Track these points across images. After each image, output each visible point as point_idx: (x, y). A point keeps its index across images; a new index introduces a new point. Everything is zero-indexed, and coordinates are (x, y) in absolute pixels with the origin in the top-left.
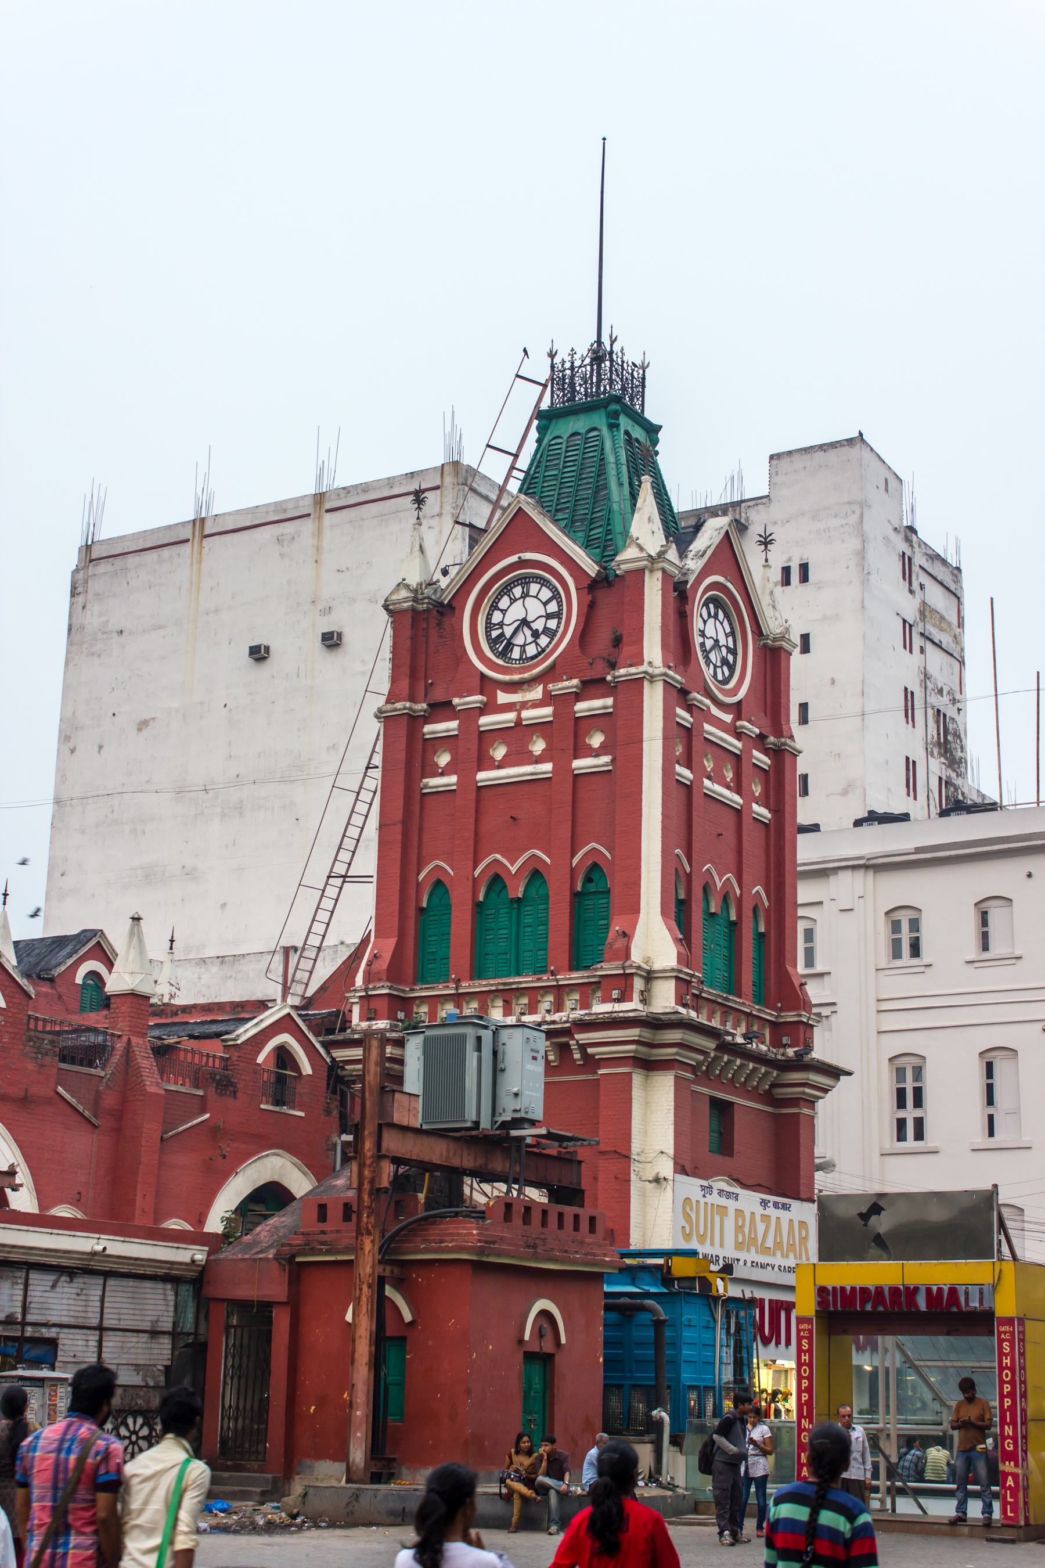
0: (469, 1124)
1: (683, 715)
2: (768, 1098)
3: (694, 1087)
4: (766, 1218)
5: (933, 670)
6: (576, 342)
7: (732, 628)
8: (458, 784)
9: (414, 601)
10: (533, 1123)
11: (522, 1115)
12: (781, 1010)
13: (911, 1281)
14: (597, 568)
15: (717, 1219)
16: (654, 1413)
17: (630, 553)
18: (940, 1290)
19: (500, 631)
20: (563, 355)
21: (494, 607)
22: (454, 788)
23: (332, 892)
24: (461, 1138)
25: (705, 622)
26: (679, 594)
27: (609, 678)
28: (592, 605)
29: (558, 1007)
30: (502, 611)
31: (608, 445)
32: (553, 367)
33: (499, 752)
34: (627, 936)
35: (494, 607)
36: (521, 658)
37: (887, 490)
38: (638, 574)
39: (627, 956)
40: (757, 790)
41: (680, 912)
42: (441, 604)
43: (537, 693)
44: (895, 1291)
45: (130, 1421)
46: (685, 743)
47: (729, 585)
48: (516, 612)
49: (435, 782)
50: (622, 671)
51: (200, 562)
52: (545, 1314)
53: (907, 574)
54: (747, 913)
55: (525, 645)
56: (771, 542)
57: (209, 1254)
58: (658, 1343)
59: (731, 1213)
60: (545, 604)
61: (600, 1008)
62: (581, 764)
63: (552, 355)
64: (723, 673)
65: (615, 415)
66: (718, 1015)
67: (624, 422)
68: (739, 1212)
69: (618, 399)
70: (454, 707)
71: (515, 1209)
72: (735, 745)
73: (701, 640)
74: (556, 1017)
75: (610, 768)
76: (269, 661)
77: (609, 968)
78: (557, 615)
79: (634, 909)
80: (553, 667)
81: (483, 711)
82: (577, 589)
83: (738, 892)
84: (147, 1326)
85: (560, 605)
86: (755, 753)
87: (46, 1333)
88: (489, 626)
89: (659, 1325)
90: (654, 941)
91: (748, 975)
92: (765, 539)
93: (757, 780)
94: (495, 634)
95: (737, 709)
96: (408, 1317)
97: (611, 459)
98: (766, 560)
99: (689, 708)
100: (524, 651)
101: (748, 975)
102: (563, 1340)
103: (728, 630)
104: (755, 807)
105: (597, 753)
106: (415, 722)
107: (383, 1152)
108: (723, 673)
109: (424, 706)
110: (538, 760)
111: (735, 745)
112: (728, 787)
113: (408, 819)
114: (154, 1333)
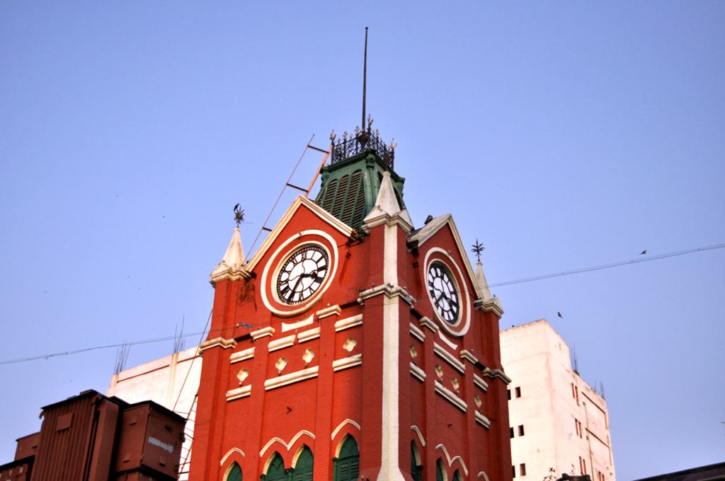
5: (593, 449)
6: (349, 128)
7: (455, 289)
8: (252, 391)
9: (229, 272)
14: (351, 229)
17: (374, 214)
19: (286, 285)
20: (339, 138)
21: (283, 270)
22: (249, 394)
25: (434, 278)
27: (359, 300)
28: (348, 256)
30: (288, 272)
32: (333, 144)
33: (281, 365)
36: (300, 300)
37: (560, 348)
38: (379, 230)
40: (479, 404)
43: (310, 320)
48: (298, 271)
49: (233, 393)
50: (368, 291)
51: (174, 376)
53: (575, 395)
55: (302, 291)
56: (481, 249)
60: (317, 262)
63: (332, 139)
64: (449, 316)
70: (252, 338)
73: (431, 289)
75: (360, 363)
79: (377, 462)
80: (319, 301)
81: (271, 338)
82: (338, 247)
83: (466, 472)
88: (279, 283)
92: (477, 247)
93: (478, 397)
94: (282, 288)
95: (459, 340)
98: (479, 260)
100: (302, 295)
103: (452, 290)
106: (223, 352)
108: (449, 316)
111: (462, 367)
112: (456, 393)
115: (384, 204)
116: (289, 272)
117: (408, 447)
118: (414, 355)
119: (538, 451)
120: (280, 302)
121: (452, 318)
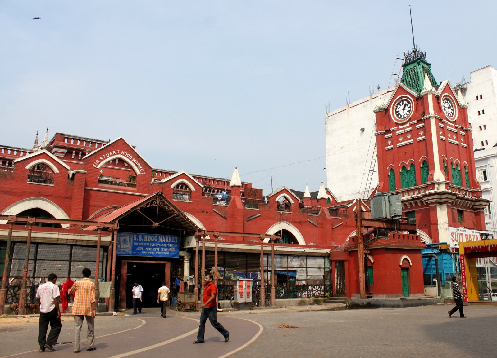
0: (384, 218)
1: (441, 125)
2: (472, 208)
3: (452, 207)
4: (473, 236)
10: (399, 216)
11: (396, 214)
12: (474, 189)
13: (486, 244)
14: (417, 95)
15: (461, 236)
16: (434, 280)
17: (424, 91)
18: (494, 246)
20: (407, 53)
21: (397, 108)
23: (371, 174)
24: (383, 221)
26: (437, 99)
27: (423, 119)
28: (417, 104)
29: (419, 193)
31: (418, 70)
32: (405, 55)
34: (432, 175)
35: (397, 108)
39: (433, 179)
41: (445, 169)
42: (385, 109)
43: (408, 125)
44: (482, 247)
45: (315, 287)
46: (442, 130)
47: (450, 95)
49: (388, 147)
51: (349, 113)
52: (405, 259)
54: (463, 168)
57: (331, 251)
58: (436, 264)
59: (464, 235)
61: (428, 192)
62: (419, 139)
63: (404, 53)
65: (419, 62)
66: (458, 191)
67: (422, 64)
68: (466, 235)
69: (419, 59)
71: (400, 236)
72: (456, 130)
74: (419, 195)
76: (364, 131)
77: (429, 183)
78: (410, 107)
79: (434, 169)
80: (410, 119)
81: (397, 130)
83: (460, 163)
84: (318, 267)
85: (410, 105)
86: (461, 132)
87: (293, 269)
88: (396, 112)
89: (436, 260)
90: (438, 175)
91: (465, 182)
94: (397, 114)
95: (455, 122)
96: (372, 261)
97: (419, 72)
99: (443, 123)
101: (465, 182)
102: (411, 264)
104: (462, 144)
105: (422, 136)
107: (362, 225)
109: (384, 131)
110: (410, 139)
111: (456, 130)
112: (455, 140)
113: (384, 155)
114: (319, 268)
115: (427, 85)
116: (399, 108)
117: (442, 161)
118: (441, 133)
119: (490, 119)
120: (397, 118)
121: (452, 115)
